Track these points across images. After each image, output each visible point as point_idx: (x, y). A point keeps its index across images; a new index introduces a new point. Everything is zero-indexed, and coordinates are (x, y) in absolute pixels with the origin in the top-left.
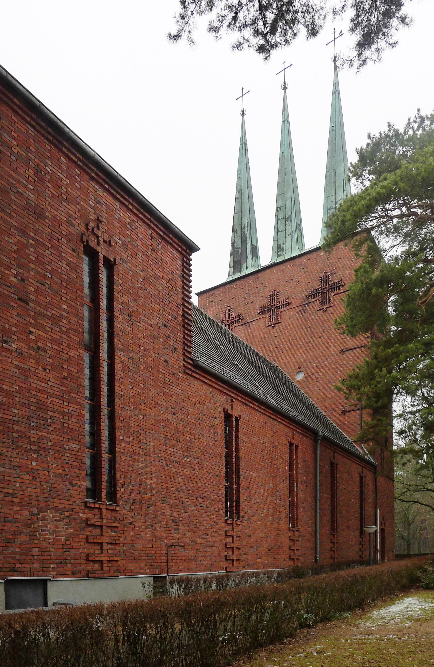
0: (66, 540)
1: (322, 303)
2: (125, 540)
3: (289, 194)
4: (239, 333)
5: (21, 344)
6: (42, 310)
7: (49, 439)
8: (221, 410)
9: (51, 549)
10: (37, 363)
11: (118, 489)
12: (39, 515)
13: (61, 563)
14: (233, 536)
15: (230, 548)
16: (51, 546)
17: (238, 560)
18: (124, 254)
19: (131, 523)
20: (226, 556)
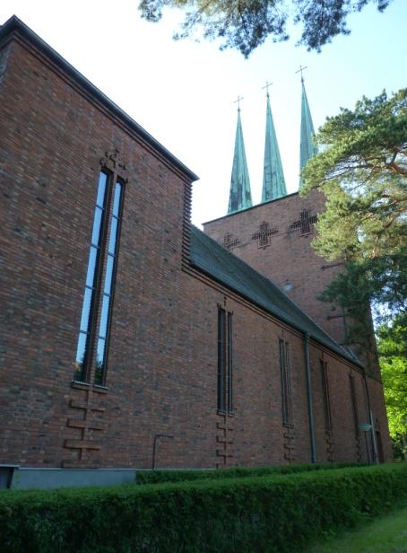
0: (45, 423)
1: (303, 231)
2: (110, 426)
3: (274, 159)
4: (236, 252)
5: (32, 234)
6: (57, 209)
7: (43, 318)
8: (215, 305)
9: (26, 432)
10: (44, 250)
11: (108, 372)
12: (19, 393)
13: (34, 448)
14: (225, 430)
15: (222, 442)
16: (25, 429)
17: (230, 456)
18: (136, 177)
19: (118, 408)
20: (217, 451)
